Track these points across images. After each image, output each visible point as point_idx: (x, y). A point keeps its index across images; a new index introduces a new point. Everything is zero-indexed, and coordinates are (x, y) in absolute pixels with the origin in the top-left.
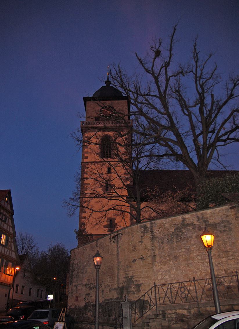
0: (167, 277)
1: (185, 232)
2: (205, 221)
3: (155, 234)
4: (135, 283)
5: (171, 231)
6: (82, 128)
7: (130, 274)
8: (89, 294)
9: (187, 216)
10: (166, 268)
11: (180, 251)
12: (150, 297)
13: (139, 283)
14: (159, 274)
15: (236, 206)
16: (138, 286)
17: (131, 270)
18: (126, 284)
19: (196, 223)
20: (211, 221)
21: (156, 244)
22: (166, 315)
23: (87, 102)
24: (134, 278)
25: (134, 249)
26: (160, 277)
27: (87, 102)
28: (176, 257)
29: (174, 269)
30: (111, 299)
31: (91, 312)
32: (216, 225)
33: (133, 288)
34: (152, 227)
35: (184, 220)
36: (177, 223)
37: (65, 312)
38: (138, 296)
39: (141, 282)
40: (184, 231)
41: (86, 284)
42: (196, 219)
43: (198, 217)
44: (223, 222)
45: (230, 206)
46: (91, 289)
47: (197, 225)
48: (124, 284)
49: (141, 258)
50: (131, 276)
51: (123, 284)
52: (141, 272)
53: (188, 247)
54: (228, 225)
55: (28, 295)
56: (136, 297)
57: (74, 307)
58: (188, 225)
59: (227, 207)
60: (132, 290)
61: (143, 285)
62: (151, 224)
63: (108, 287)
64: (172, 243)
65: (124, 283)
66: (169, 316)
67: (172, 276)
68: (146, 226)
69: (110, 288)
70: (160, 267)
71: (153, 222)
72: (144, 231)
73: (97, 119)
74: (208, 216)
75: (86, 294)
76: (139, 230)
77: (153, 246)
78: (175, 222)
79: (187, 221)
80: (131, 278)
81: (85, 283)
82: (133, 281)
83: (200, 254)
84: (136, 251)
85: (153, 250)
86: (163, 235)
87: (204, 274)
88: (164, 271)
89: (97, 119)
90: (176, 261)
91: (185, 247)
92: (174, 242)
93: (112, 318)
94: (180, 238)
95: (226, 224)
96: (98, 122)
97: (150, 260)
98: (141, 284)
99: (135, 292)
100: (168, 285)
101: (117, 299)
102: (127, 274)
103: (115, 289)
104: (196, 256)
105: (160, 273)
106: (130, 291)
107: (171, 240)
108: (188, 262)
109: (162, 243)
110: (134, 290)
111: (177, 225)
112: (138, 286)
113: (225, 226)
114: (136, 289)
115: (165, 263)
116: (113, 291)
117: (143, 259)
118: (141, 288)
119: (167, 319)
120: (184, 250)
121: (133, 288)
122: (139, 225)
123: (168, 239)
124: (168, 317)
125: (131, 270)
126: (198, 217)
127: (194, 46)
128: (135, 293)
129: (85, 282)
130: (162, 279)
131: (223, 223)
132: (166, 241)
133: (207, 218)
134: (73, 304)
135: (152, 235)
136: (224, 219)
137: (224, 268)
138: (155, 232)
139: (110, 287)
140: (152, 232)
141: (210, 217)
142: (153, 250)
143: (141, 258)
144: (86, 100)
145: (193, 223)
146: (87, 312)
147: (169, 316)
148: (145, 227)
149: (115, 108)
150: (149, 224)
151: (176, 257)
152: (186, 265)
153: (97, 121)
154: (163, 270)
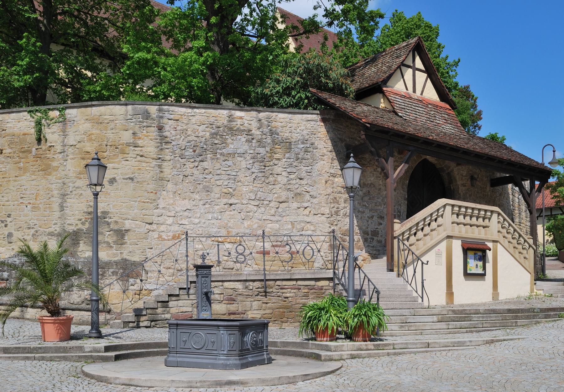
1: (232, 144)
2: (272, 133)
4: (112, 226)
12: (370, 283)
15: (329, 118)
16: (121, 234)
25: (114, 155)
28: (208, 190)
33: (107, 235)
35: (231, 119)
37: (64, 344)
42: (255, 124)
48: (80, 226)
49: (132, 179)
51: (77, 225)
55: (453, 221)
62: (160, 110)
63: (29, 228)
65: (83, 224)
69: (37, 232)
98: (127, 231)
100: (308, 248)
110: (110, 241)
112: (121, 234)
114: (115, 238)
117: (135, 180)
118: (126, 238)
138: (167, 129)
140: (160, 129)
143: (132, 179)
148: (147, 115)
150: (156, 109)
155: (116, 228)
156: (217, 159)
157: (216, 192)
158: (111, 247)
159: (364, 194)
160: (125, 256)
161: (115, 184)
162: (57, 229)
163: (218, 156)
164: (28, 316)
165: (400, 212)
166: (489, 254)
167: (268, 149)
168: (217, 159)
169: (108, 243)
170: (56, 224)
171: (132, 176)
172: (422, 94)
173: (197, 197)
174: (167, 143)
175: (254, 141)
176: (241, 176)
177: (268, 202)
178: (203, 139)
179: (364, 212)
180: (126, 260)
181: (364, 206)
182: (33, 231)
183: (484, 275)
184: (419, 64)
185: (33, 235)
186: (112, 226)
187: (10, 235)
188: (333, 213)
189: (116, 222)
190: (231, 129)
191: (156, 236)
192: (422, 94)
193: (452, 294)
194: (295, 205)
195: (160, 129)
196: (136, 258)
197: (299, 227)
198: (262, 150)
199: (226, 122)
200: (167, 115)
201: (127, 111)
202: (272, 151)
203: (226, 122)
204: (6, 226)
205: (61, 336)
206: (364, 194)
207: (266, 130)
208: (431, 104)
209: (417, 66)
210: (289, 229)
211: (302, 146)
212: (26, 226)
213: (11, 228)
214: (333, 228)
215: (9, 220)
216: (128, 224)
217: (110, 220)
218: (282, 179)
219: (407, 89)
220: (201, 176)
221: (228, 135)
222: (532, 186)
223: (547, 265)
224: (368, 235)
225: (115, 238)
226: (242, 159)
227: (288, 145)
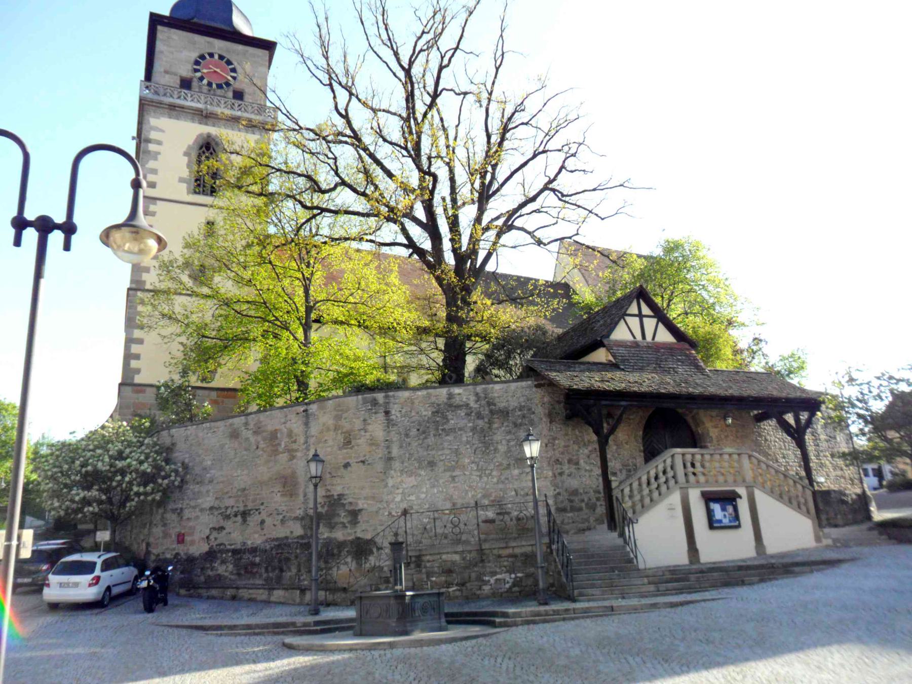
0: (413, 498)
1: (452, 419)
3: (393, 417)
4: (347, 508)
5: (425, 416)
6: (143, 102)
7: (337, 490)
8: (222, 528)
9: (457, 390)
10: (411, 481)
11: (440, 453)
13: (357, 509)
14: (397, 491)
15: (544, 384)
16: (355, 514)
17: (339, 484)
18: (326, 508)
19: (472, 404)
20: (502, 405)
21: (395, 437)
22: (423, 563)
23: (159, 28)
24: (345, 499)
26: (398, 499)
27: (159, 28)
28: (432, 464)
29: (426, 484)
30: (287, 538)
31: (228, 564)
32: (508, 413)
34: (388, 403)
35: (450, 396)
36: (437, 401)
38: (353, 531)
39: (360, 506)
40: (450, 417)
41: (211, 508)
42: (473, 398)
43: (477, 394)
44: (521, 408)
45: (536, 383)
46: (228, 517)
47: (475, 408)
49: (363, 462)
50: (338, 495)
52: (362, 488)
53: (456, 447)
54: (528, 415)
56: (349, 534)
57: (172, 557)
58: (458, 407)
59: (530, 382)
60: (342, 520)
61: (363, 512)
62: (387, 397)
63: (278, 514)
64: (426, 438)
66: (428, 565)
67: (423, 496)
68: (375, 399)
69: (284, 517)
70: (399, 479)
71: (391, 394)
72: (371, 409)
73: (186, 84)
74: (496, 395)
75: (214, 529)
76: (360, 406)
77: (387, 440)
78: (433, 399)
79: (457, 401)
80: (340, 499)
81: (207, 505)
82: (343, 504)
83: (477, 460)
84: (353, 446)
85: (388, 447)
86: (408, 421)
87: (480, 495)
88: (407, 488)
89: (186, 84)
90: (432, 470)
91: (449, 447)
92: (429, 435)
93: (289, 574)
94: (443, 430)
95: (525, 412)
96: (189, 95)
97: (379, 466)
98: (360, 510)
99: (347, 525)
101: (302, 537)
102: (329, 491)
103: (296, 518)
104: (469, 464)
105: (400, 491)
106: (336, 523)
107: (424, 432)
108: (454, 474)
109: (407, 435)
111: (438, 405)
112: (355, 514)
113: (524, 417)
114: (349, 519)
115: (411, 474)
116: (291, 523)
117: (367, 463)
118: (359, 517)
119: (424, 570)
120: (447, 452)
121: (343, 517)
122: (360, 397)
123: (418, 430)
124: (426, 567)
125: (339, 484)
126: (477, 394)
127: (584, 171)
128: (346, 527)
129: (208, 501)
130: (402, 501)
131: (520, 410)
132: (414, 432)
133: (493, 398)
134: (167, 549)
135: (387, 420)
136: (523, 404)
137: (515, 487)
139: (284, 513)
140: (387, 413)
141: (499, 397)
142: (388, 447)
143: (363, 462)
144: (155, 21)
145: (467, 405)
146: (216, 565)
147: (428, 565)
148: (375, 403)
149: (235, 64)
151: (432, 464)
152: (450, 479)
153: (186, 91)
154: (404, 486)
155: (351, 508)
156: (440, 435)
157: (440, 467)
158: (346, 527)
159: (590, 451)
160: (359, 535)
161: (349, 468)
162: (299, 513)
163: (440, 432)
164: (273, 599)
165: (636, 466)
166: (743, 506)
167: (486, 420)
168: (440, 435)
169: (343, 523)
170: (300, 508)
171: (363, 459)
172: (654, 338)
173: (423, 473)
174: (393, 425)
175: (473, 414)
176: (462, 449)
177: (489, 472)
178: (426, 418)
179: (591, 470)
180: (358, 538)
181: (591, 464)
182: (281, 517)
183: (739, 526)
184: (646, 310)
185: (282, 520)
186: (347, 508)
187: (263, 522)
188: (556, 474)
189: (351, 503)
190: (450, 406)
191: (386, 513)
192: (654, 338)
193: (696, 551)
194: (516, 472)
195: (387, 413)
196: (368, 536)
197: (522, 493)
198: (480, 423)
199: (445, 400)
200: (392, 400)
201: (357, 401)
202: (490, 423)
203: (445, 400)
204: (260, 513)
205: (568, 411)
206: (590, 451)
207: (483, 402)
208: (662, 348)
209: (637, 319)
210: (512, 496)
211: (519, 413)
212: (275, 512)
213: (264, 515)
214: (558, 491)
215: (262, 507)
216: (361, 504)
217: (345, 502)
218: (502, 448)
219: (634, 337)
220: (425, 453)
221: (448, 411)
222: (797, 420)
223: (174, 679)
224: (599, 493)
225: (349, 519)
226: (462, 432)
227: (505, 414)
